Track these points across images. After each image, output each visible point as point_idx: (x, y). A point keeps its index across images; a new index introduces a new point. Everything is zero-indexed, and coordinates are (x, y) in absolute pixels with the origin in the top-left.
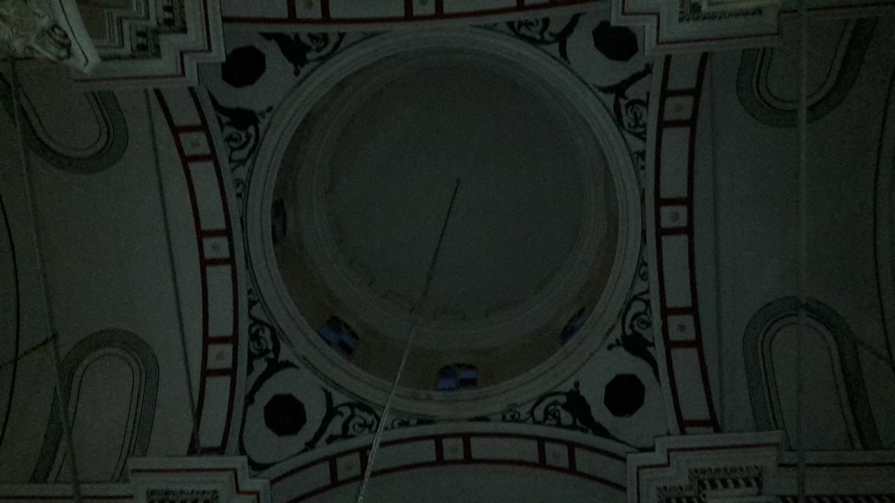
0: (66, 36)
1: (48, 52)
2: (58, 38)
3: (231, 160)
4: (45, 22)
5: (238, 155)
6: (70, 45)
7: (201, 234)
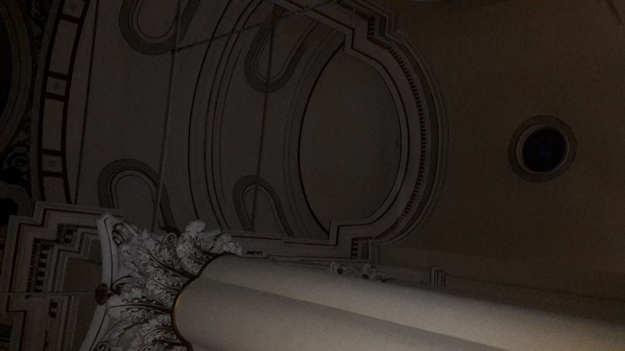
0: (114, 238)
1: (129, 230)
2: (120, 238)
3: (28, 148)
4: (125, 247)
5: (23, 149)
6: (113, 232)
7: (65, 99)
